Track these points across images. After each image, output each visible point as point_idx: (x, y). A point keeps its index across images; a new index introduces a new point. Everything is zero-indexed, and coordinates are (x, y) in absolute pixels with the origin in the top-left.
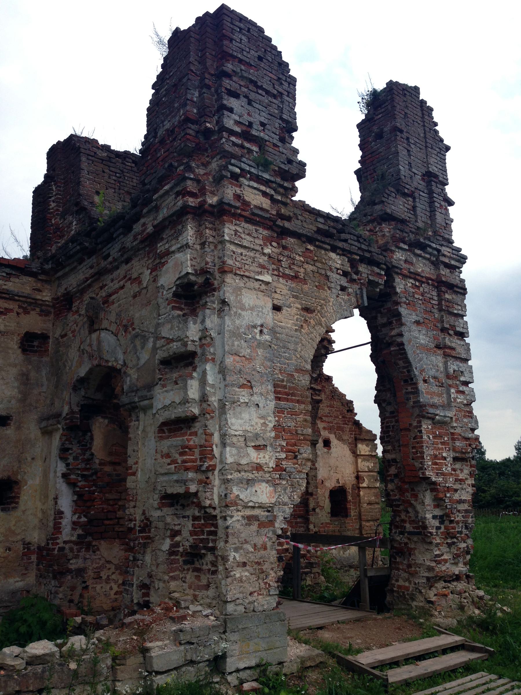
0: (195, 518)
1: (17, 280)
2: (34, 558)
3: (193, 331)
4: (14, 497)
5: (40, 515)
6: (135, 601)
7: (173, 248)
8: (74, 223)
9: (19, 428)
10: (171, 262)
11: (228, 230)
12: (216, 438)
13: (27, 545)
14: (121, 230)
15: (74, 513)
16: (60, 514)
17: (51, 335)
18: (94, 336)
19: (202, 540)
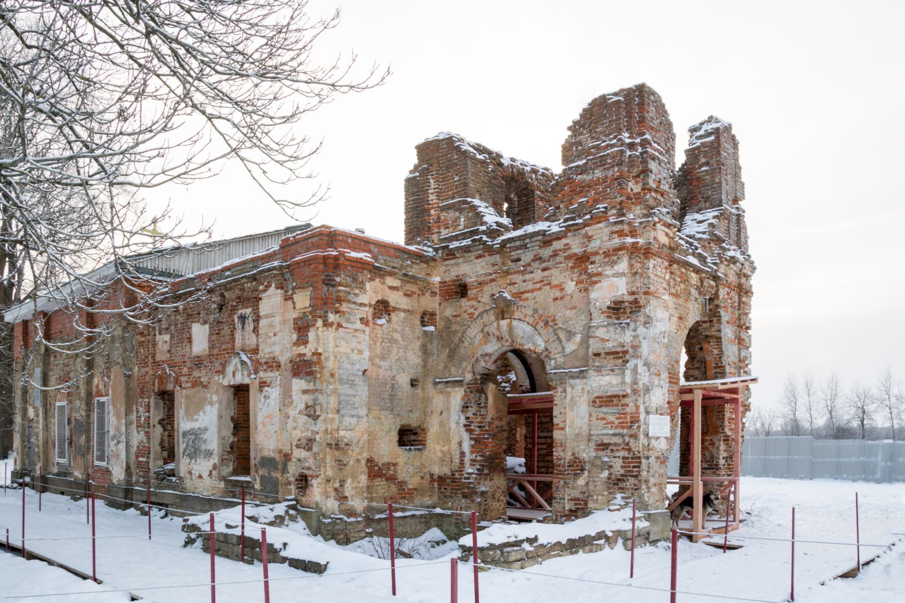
0: (624, 458)
1: (417, 267)
2: (436, 484)
3: (627, 337)
4: (421, 441)
5: (439, 454)
6: (567, 508)
7: (607, 273)
8: (462, 220)
9: (423, 388)
10: (605, 283)
11: (651, 263)
12: (642, 409)
13: (432, 475)
14: (538, 243)
15: (472, 452)
16: (463, 454)
17: (438, 312)
18: (504, 323)
19: (629, 471)
